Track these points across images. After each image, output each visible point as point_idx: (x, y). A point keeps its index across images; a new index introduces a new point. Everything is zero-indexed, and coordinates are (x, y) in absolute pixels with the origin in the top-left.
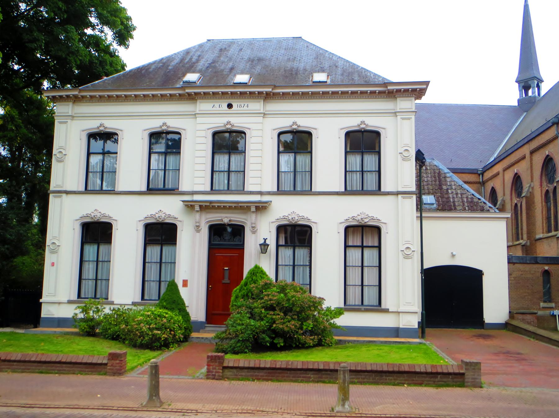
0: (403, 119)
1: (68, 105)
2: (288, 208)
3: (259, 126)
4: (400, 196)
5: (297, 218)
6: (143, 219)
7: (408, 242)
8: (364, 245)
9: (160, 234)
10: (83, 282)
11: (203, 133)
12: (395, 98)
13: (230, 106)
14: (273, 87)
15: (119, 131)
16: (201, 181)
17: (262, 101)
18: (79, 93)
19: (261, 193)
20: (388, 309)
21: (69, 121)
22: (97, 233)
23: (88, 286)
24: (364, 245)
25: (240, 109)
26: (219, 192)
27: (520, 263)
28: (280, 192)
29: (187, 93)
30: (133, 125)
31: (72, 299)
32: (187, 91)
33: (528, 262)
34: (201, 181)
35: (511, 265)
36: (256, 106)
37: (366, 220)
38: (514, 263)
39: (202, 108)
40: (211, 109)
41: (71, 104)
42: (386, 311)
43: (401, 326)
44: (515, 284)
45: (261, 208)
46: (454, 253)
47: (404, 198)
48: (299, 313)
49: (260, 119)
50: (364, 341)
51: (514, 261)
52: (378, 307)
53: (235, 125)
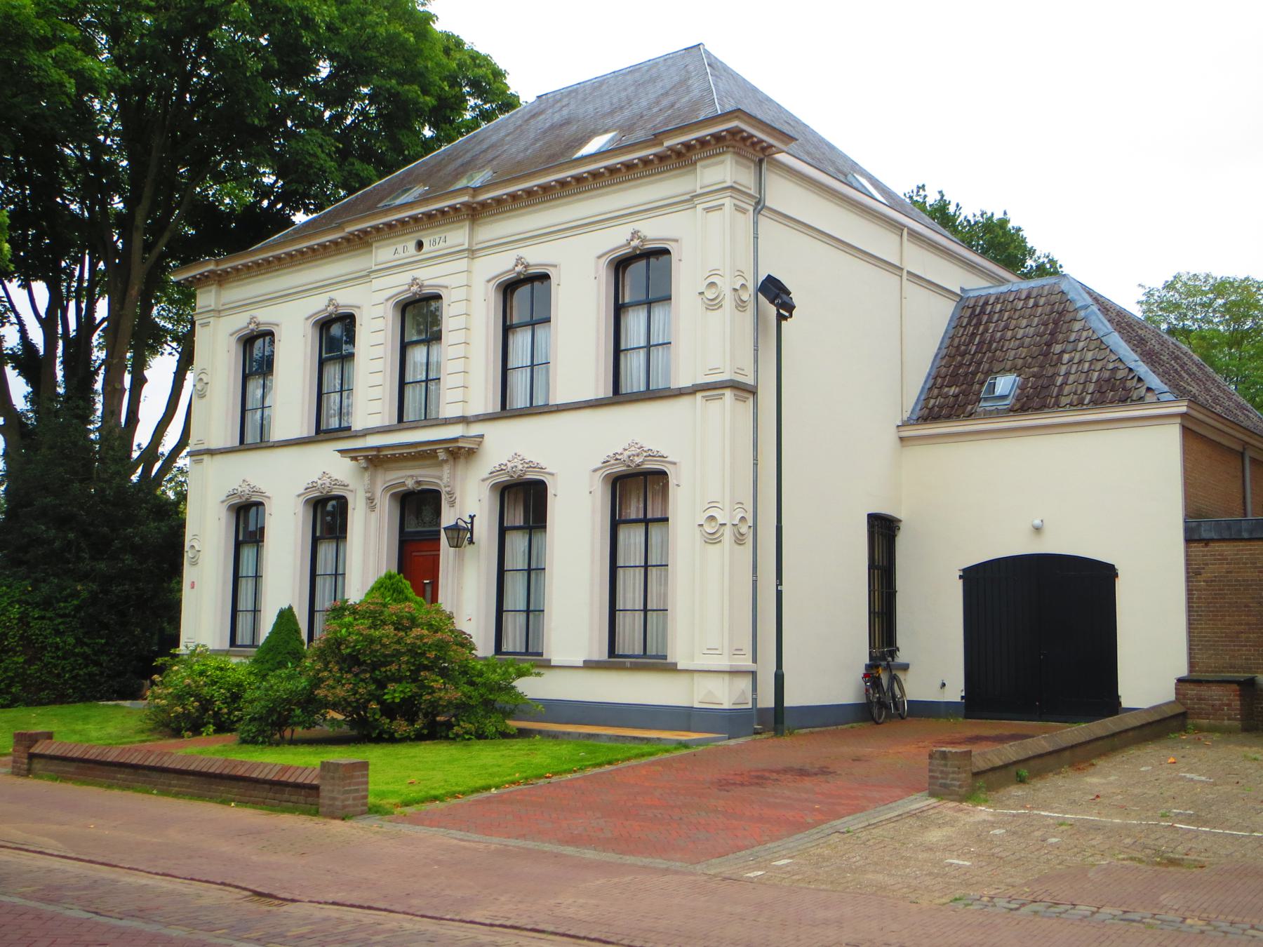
0: (708, 210)
1: (723, 162)
2: (509, 447)
3: (462, 279)
4: (699, 395)
5: (520, 467)
6: (600, 465)
7: (713, 505)
8: (649, 516)
9: (328, 516)
10: (619, 615)
11: (379, 310)
12: (368, 245)
13: (420, 245)
14: (471, 191)
15: (672, 244)
16: (377, 406)
17: (467, 223)
18: (474, 196)
19: (464, 420)
20: (675, 664)
21: (211, 320)
22: (247, 519)
23: (630, 627)
24: (649, 516)
25: (437, 247)
26: (415, 426)
27: (1223, 540)
28: (506, 411)
29: (670, 148)
30: (574, 249)
31: (596, 657)
32: (667, 143)
33: (1246, 535)
34: (377, 406)
35: (1198, 548)
36: (458, 236)
37: (638, 460)
38: (1207, 542)
39: (707, 181)
40: (391, 257)
41: (214, 288)
42: (672, 668)
43: (697, 705)
44: (1207, 602)
45: (460, 453)
46: (1037, 522)
47: (708, 399)
48: (374, 667)
49: (462, 264)
50: (580, 734)
51: (1205, 535)
52: (654, 661)
53: (426, 283)
